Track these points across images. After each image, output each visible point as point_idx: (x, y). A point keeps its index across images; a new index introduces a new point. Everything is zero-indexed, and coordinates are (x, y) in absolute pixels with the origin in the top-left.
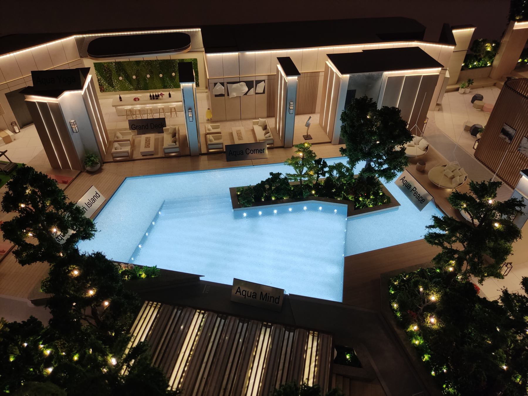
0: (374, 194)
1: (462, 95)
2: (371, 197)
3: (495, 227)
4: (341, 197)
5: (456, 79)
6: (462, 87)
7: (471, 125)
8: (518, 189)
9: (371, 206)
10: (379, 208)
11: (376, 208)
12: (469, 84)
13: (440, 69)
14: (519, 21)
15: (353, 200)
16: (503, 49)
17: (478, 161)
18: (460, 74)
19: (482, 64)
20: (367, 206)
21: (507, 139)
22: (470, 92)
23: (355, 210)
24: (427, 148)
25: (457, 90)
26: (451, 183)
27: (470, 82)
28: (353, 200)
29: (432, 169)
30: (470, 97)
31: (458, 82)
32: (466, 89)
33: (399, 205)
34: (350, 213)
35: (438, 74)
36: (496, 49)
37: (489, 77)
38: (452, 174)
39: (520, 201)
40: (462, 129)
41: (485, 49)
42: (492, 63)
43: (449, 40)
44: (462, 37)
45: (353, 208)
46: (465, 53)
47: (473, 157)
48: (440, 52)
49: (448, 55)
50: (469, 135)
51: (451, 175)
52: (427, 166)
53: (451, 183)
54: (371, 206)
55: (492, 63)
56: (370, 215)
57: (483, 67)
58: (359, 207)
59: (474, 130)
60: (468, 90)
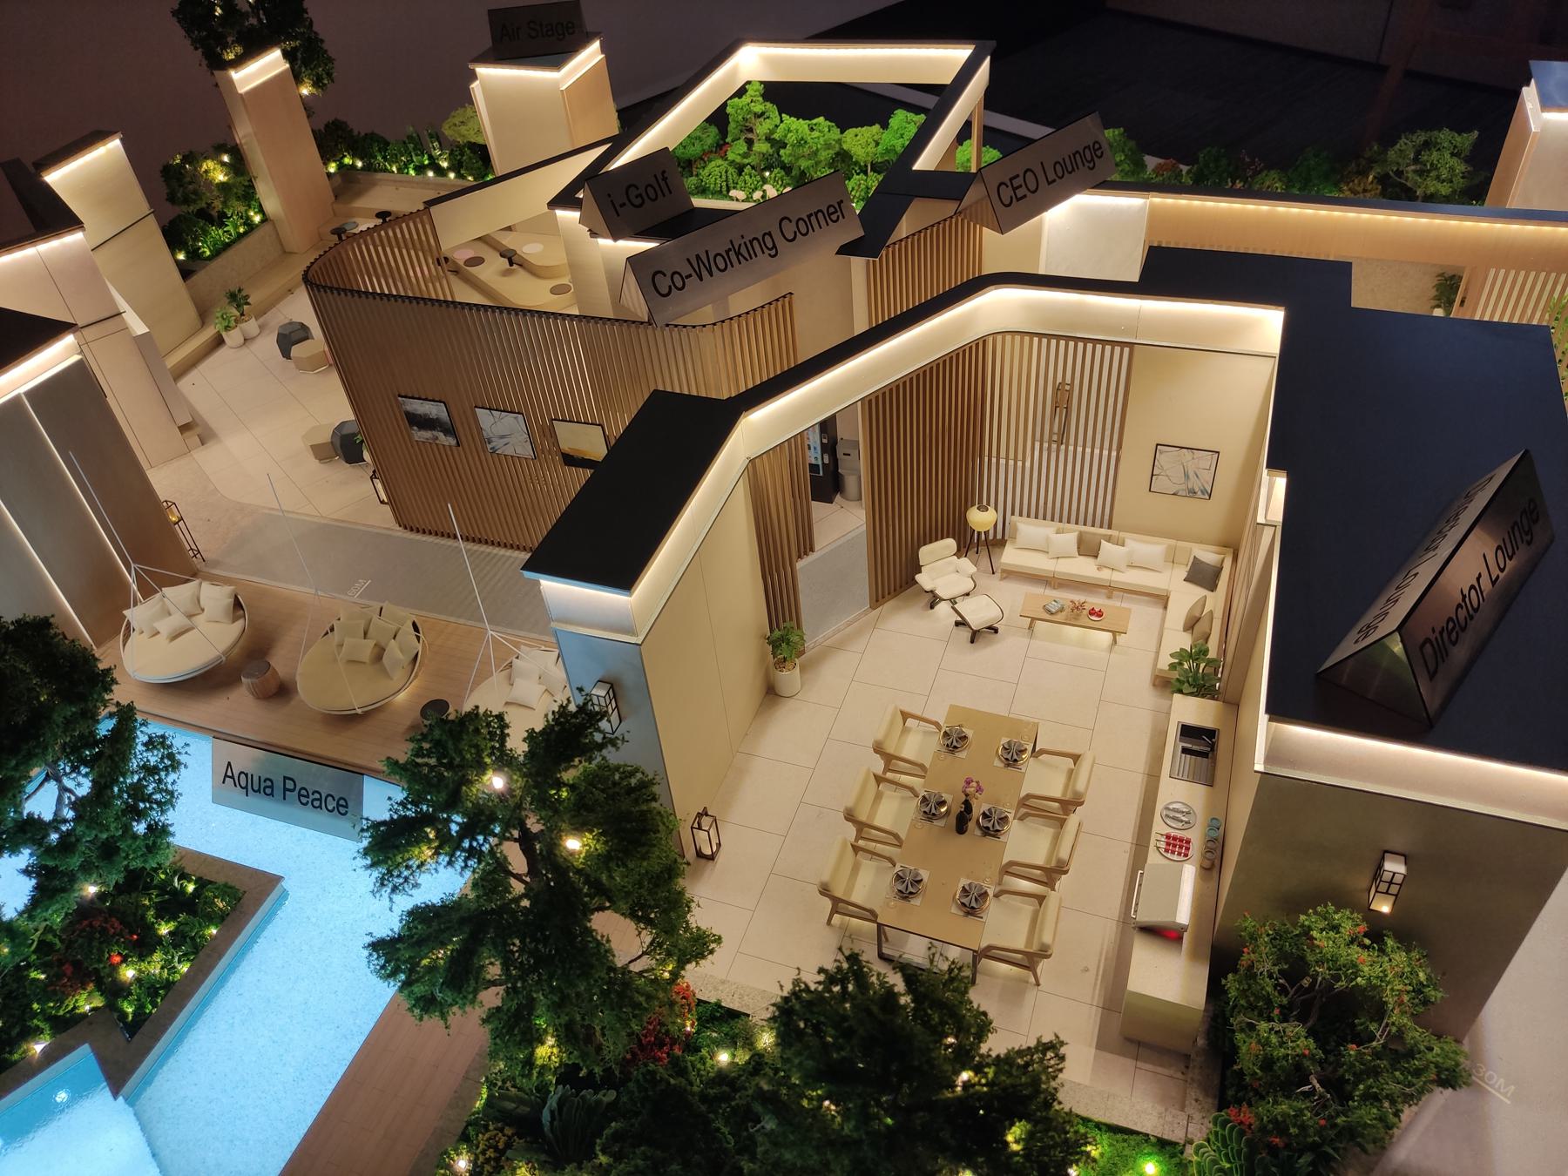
0: (164, 912)
1: (245, 351)
2: (164, 929)
3: (572, 853)
4: (38, 1031)
5: (191, 312)
6: (227, 328)
7: (325, 436)
8: (559, 621)
9: (184, 968)
10: (218, 950)
11: (206, 958)
12: (238, 307)
13: (69, 340)
14: (239, 62)
15: (98, 1002)
16: (258, 159)
17: (419, 537)
18: (189, 289)
19: (236, 227)
20: (168, 985)
21: (441, 436)
22: (262, 327)
23: (128, 1043)
24: (237, 605)
25: (219, 342)
26: (385, 673)
27: (237, 298)
28: (98, 1002)
29: (300, 670)
30: (268, 345)
31: (203, 315)
32: (244, 325)
33: (274, 880)
34: (119, 1074)
35: (76, 358)
36: (239, 165)
37: (286, 253)
38: (370, 643)
39: (581, 709)
40: (314, 463)
41: (209, 183)
42: (261, 210)
43: (52, 216)
44: (92, 185)
45: (120, 1037)
46: (152, 228)
47: (400, 532)
48: (49, 273)
49: (83, 272)
50: (341, 470)
51: (366, 649)
52: (279, 662)
53: (385, 673)
54: (184, 968)
55: (261, 210)
56: (205, 1004)
57: (245, 233)
58: (140, 1008)
59: (346, 447)
60: (251, 326)
